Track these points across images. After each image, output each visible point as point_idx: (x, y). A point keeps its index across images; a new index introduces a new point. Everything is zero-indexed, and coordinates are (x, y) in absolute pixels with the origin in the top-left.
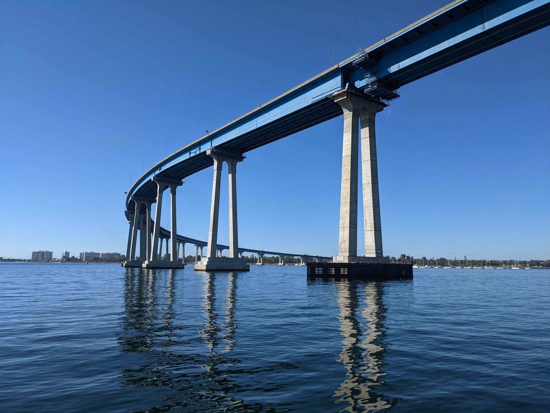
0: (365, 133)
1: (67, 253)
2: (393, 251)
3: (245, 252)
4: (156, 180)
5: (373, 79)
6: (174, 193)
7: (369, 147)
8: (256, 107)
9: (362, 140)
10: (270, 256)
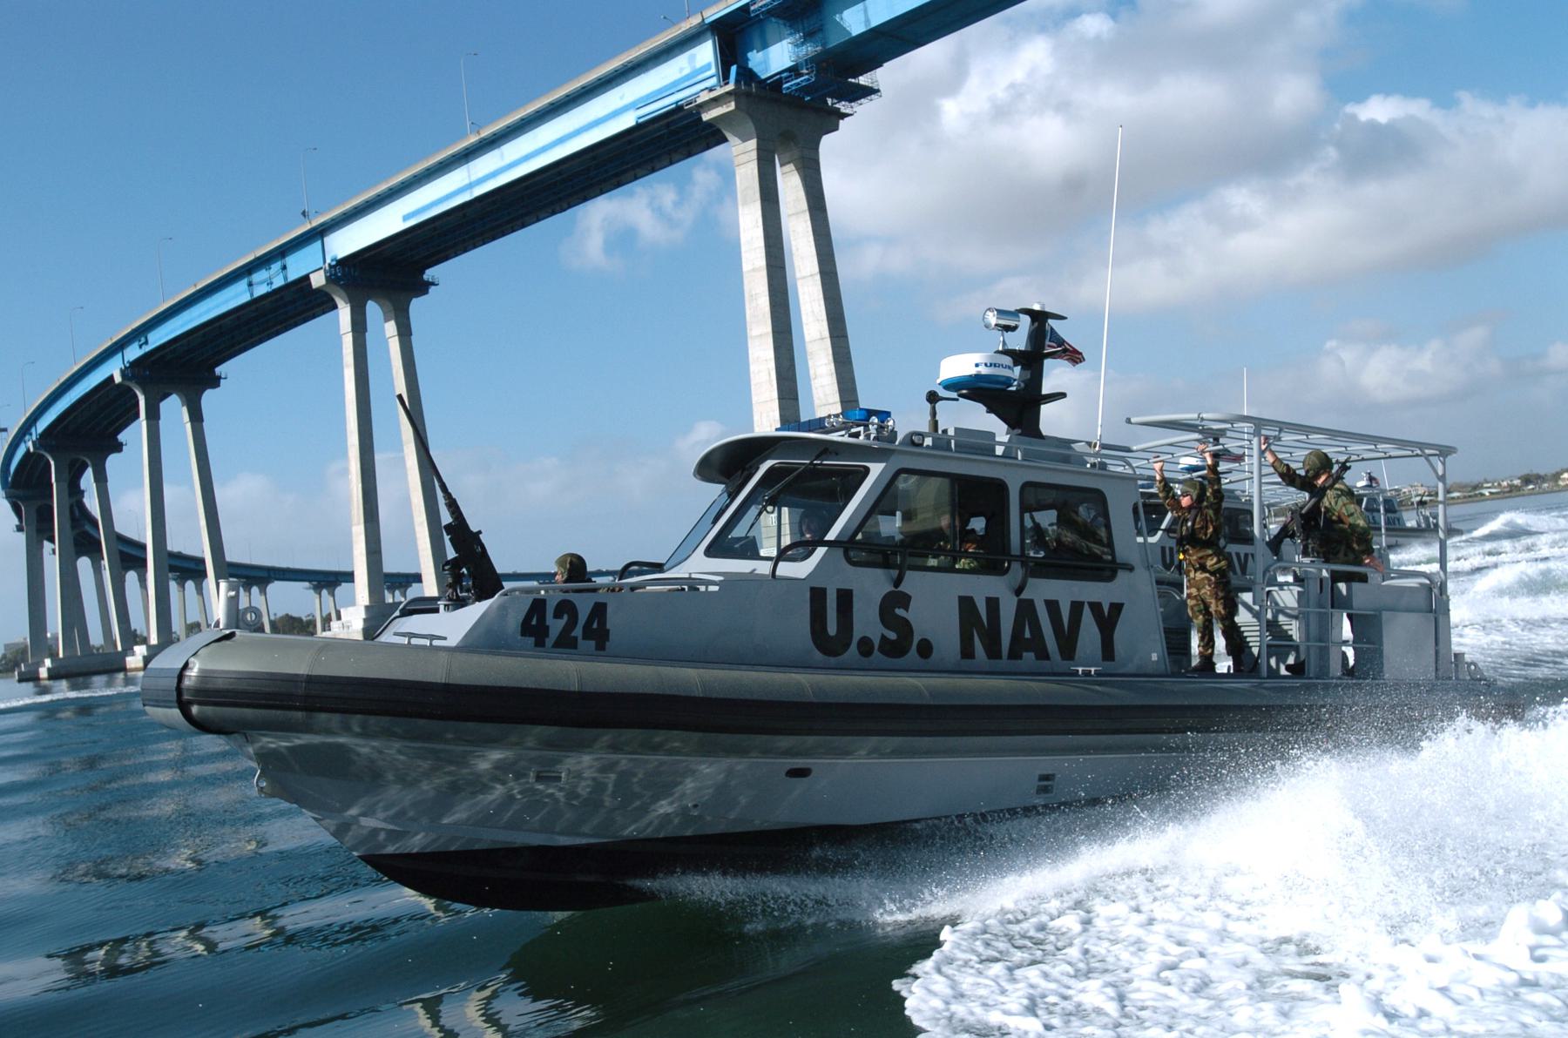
0: (790, 184)
4: (130, 379)
5: (809, 49)
7: (811, 238)
8: (464, 136)
9: (799, 283)
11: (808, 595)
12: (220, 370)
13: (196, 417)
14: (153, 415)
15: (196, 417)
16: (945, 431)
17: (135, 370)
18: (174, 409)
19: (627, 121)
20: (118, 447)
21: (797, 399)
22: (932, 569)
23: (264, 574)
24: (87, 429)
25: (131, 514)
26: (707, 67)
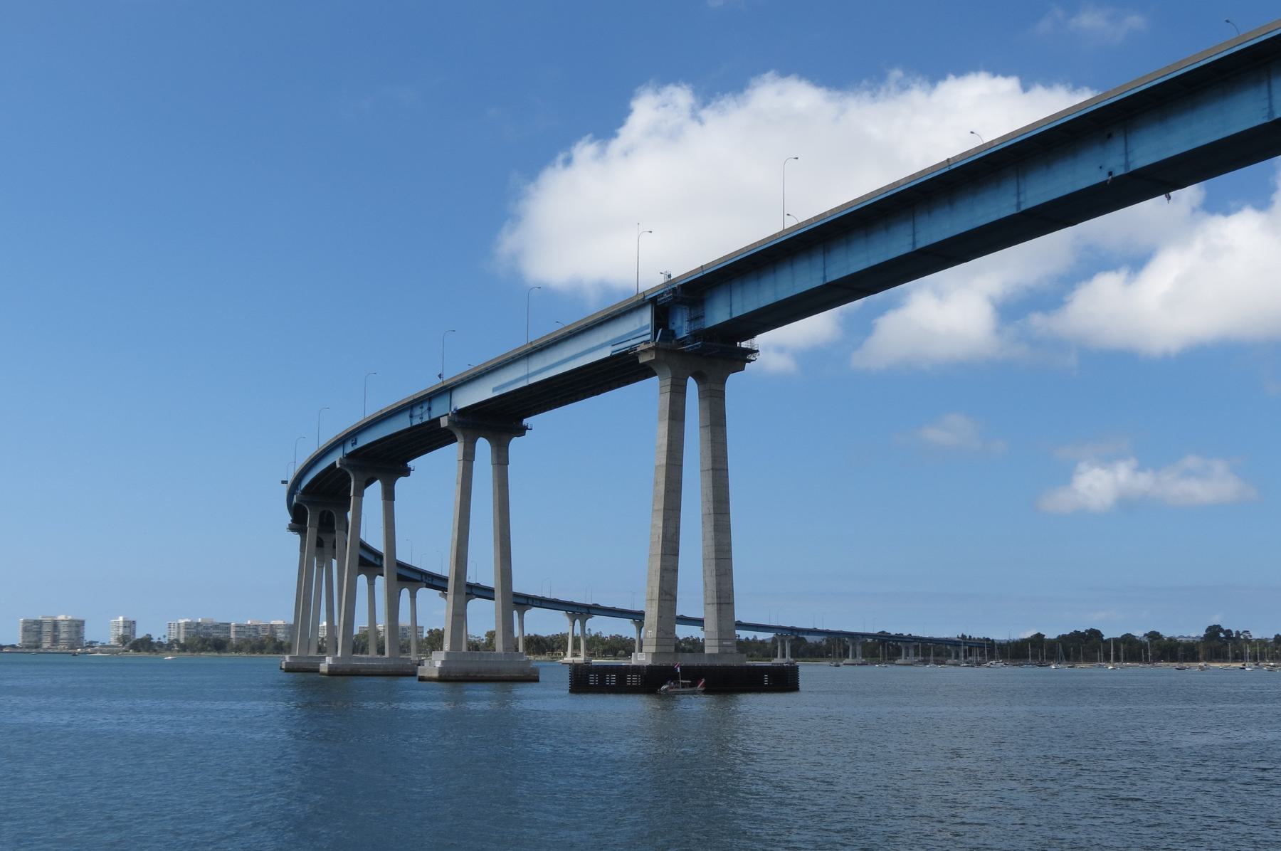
1: (130, 625)
2: (778, 591)
3: (596, 618)
4: (348, 465)
6: (389, 495)
10: (817, 639)
11: (801, 684)
12: (411, 464)
18: (483, 447)
19: (605, 353)
21: (677, 555)
22: (169, 664)
23: (524, 601)
26: (646, 327)
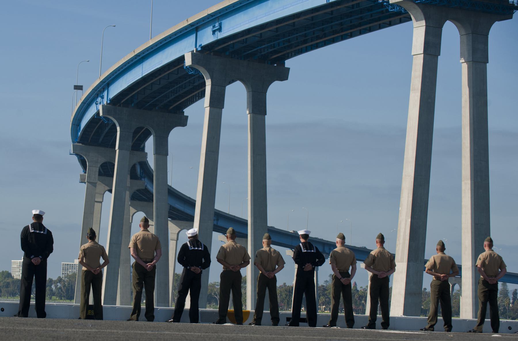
13: (258, 107)
14: (218, 102)
15: (258, 107)
16: (425, 289)
17: (204, 53)
20: (183, 122)
24: (156, 101)
25: (185, 174)
